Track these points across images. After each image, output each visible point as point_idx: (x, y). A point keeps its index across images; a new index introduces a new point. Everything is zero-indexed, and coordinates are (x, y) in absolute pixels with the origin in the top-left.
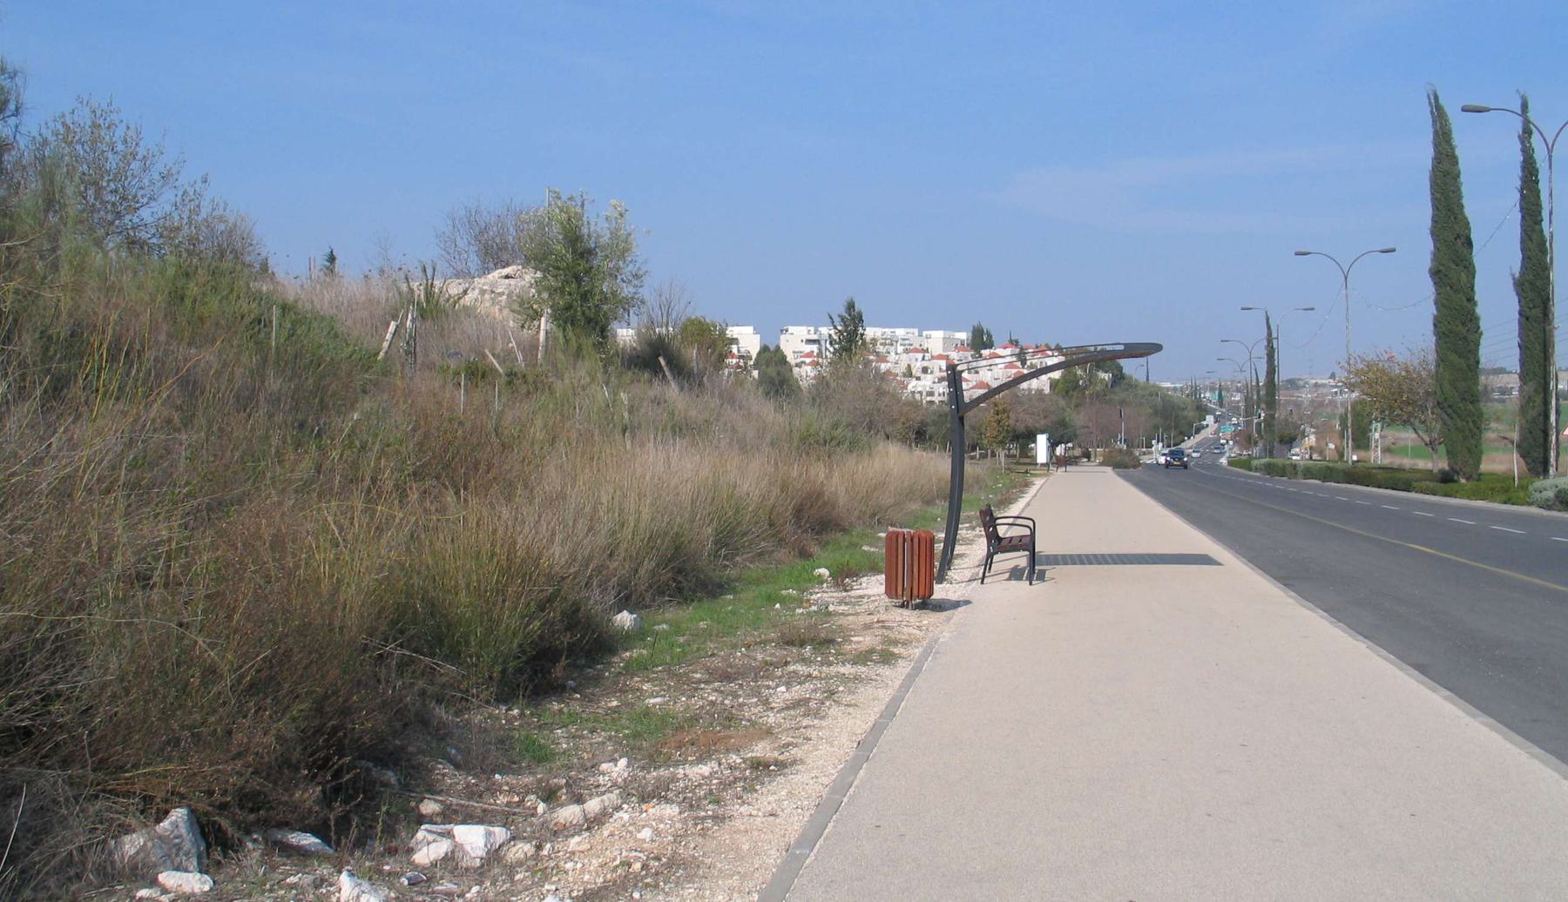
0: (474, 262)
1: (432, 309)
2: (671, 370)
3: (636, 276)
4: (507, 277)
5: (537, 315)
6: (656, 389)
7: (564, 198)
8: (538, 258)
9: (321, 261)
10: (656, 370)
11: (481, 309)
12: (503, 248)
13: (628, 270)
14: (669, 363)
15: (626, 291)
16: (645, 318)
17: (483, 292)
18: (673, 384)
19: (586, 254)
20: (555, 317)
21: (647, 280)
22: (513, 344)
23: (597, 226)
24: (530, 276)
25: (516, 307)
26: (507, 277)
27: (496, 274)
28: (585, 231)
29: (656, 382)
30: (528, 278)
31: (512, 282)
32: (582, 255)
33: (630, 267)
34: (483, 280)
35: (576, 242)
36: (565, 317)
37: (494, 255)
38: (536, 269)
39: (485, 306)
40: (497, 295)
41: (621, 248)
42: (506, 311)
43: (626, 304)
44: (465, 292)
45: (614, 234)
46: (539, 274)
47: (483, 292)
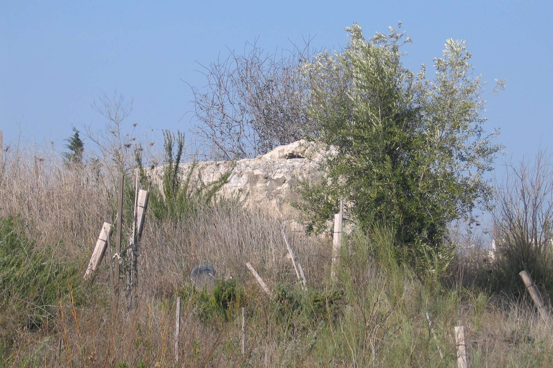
0: (250, 136)
1: (175, 204)
2: (540, 290)
3: (483, 152)
4: (292, 156)
5: (329, 211)
6: (513, 321)
7: (369, 35)
8: (335, 128)
9: (63, 147)
10: (518, 292)
11: (249, 204)
12: (292, 116)
13: (468, 142)
14: (536, 277)
15: (466, 173)
16: (499, 212)
17: (253, 179)
18: (542, 312)
19: (407, 117)
20: (362, 211)
21: (498, 160)
22: (290, 256)
23: (421, 74)
24: (323, 153)
25: (301, 201)
26: (292, 156)
27: (277, 152)
28: (403, 85)
29: (515, 310)
30: (318, 157)
31: (297, 162)
32: (398, 119)
33: (472, 139)
34: (253, 162)
35: (384, 94)
36: (369, 212)
37: (276, 125)
38: (329, 142)
39: (256, 199)
40: (269, 186)
41: (455, 111)
42: (287, 208)
43: (469, 192)
44: (224, 179)
45: (448, 90)
46: (334, 151)
47: (253, 179)
